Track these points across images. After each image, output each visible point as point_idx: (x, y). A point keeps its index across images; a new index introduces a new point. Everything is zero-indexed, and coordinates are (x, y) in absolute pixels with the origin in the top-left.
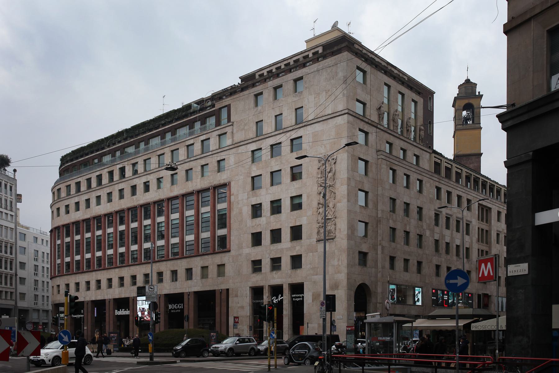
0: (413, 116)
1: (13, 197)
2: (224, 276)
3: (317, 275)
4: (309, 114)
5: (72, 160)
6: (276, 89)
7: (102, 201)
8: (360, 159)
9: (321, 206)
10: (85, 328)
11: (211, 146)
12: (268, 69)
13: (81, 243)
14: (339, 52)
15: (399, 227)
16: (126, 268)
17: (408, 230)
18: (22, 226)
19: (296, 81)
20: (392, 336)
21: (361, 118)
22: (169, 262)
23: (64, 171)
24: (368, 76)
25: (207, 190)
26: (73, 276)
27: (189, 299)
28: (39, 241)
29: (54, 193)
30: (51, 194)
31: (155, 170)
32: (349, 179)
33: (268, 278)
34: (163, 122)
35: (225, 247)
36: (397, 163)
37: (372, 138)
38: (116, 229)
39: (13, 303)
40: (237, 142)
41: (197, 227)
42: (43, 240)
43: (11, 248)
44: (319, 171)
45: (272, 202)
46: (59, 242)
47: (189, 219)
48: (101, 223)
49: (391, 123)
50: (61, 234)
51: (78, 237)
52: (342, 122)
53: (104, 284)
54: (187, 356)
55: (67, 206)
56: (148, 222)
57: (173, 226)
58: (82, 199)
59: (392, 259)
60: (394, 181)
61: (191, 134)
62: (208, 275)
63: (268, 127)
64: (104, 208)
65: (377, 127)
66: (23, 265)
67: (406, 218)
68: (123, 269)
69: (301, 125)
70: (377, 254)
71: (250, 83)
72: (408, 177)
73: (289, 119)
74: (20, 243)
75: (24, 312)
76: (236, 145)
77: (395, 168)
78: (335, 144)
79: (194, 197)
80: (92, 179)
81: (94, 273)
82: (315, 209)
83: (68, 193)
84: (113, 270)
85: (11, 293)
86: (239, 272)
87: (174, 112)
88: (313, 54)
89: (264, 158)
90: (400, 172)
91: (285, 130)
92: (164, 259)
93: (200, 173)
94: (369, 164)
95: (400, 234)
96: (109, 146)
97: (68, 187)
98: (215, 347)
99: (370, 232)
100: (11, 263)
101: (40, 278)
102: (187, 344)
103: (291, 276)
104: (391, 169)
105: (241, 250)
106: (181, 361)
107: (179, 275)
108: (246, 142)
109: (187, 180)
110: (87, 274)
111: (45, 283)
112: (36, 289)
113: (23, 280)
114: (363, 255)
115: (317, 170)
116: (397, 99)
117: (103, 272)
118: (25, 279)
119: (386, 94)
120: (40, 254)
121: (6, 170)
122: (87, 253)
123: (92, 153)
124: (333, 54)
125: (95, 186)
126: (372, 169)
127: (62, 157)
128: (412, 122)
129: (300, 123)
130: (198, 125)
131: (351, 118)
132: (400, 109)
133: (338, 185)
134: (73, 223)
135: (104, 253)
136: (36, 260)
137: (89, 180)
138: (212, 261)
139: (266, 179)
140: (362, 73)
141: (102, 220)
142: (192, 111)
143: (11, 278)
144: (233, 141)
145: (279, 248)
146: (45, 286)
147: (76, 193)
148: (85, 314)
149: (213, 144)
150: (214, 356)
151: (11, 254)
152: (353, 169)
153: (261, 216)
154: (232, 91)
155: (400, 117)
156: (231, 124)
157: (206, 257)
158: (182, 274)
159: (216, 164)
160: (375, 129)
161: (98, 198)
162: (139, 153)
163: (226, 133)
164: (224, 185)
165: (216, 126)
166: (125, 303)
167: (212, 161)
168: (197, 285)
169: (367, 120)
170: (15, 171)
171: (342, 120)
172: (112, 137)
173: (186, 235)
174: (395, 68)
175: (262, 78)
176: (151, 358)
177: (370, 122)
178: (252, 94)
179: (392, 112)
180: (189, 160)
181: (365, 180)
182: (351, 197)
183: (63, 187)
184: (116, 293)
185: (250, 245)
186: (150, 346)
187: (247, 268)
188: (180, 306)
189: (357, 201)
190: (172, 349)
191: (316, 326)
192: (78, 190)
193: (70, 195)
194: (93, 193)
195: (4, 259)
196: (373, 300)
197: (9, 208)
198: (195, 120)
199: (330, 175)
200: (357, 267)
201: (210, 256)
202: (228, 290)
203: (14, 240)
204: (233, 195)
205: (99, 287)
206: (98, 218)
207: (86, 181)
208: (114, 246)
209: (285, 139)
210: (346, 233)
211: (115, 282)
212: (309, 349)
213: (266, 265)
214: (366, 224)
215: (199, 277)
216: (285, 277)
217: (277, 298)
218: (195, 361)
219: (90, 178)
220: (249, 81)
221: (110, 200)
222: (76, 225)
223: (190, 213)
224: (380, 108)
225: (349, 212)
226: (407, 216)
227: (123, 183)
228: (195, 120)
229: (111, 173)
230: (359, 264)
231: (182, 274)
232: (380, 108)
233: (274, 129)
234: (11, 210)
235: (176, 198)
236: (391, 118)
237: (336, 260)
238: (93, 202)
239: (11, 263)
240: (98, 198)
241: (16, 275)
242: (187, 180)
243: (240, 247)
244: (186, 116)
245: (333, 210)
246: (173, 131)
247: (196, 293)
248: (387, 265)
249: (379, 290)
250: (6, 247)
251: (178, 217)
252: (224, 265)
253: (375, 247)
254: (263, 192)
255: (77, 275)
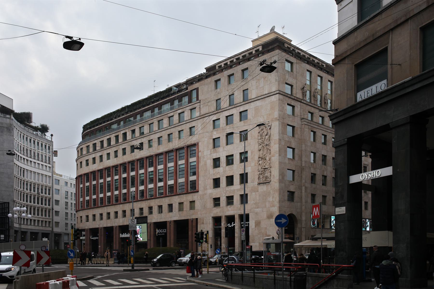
0: (329, 92)
1: (51, 154)
2: (194, 209)
3: (258, 208)
4: (252, 94)
5: (90, 128)
6: (229, 76)
7: (111, 157)
8: (288, 125)
9: (260, 159)
10: (100, 247)
11: (185, 117)
12: (225, 62)
13: (97, 186)
14: (273, 50)
15: (319, 173)
16: (128, 204)
17: (325, 175)
18: (57, 174)
19: (243, 71)
20: (280, 252)
21: (289, 96)
22: (157, 200)
23: (85, 136)
24: (294, 66)
25: (182, 148)
26: (91, 210)
27: (170, 226)
28: (69, 185)
29: (78, 151)
30: (76, 152)
31: (177, 125)
32: (280, 140)
33: (225, 211)
34: (153, 100)
35: (195, 189)
36: (316, 127)
37: (297, 110)
38: (120, 177)
39: (50, 229)
40: (203, 114)
41: (175, 174)
42: (71, 184)
43: (49, 190)
44: (259, 134)
45: (227, 157)
46: (81, 186)
47: (170, 169)
48: (110, 172)
49: (312, 98)
50: (83, 180)
51: (94, 183)
52: (275, 100)
53: (112, 215)
54: (160, 266)
55: (87, 161)
56: (142, 171)
57: (160, 174)
58: (97, 155)
59: (313, 196)
60: (314, 140)
61: (171, 109)
62: (183, 209)
63: (225, 104)
64: (112, 162)
65: (301, 102)
66: (57, 202)
67: (324, 166)
68: (125, 204)
69: (247, 102)
70: (302, 192)
71: (212, 72)
72: (325, 136)
73: (238, 97)
74: (56, 187)
75: (58, 235)
76: (202, 117)
77: (315, 130)
78: (270, 115)
79: (174, 154)
80: (136, 130)
81: (105, 208)
82: (257, 162)
83: (88, 151)
84: (118, 206)
85: (49, 222)
86: (204, 206)
87: (161, 93)
88: (256, 51)
89: (221, 126)
90: (319, 133)
91: (236, 106)
92: (153, 197)
93: (157, 142)
94: (296, 128)
95: (319, 179)
96: (115, 118)
97: (88, 147)
98: (180, 260)
99: (296, 177)
100: (49, 201)
101: (69, 211)
102: (160, 257)
103: (240, 209)
104: (312, 131)
105: (206, 190)
106: (154, 269)
107: (163, 209)
108: (209, 114)
109: (169, 141)
110: (100, 208)
111: (73, 215)
112: (66, 219)
113: (57, 213)
114: (291, 194)
115: (257, 134)
116: (317, 81)
117: (111, 207)
118: (59, 212)
119: (308, 78)
120: (69, 194)
121: (45, 135)
122: (100, 193)
123: (104, 122)
124: (269, 51)
125: (138, 135)
126: (298, 132)
127: (84, 126)
128: (329, 97)
129: (192, 119)
130: (176, 102)
131: (281, 97)
132: (319, 87)
133: (272, 144)
134: (91, 172)
135: (112, 193)
136: (67, 198)
137: (102, 142)
138: (186, 199)
139: (223, 140)
140: (290, 64)
141: (111, 170)
142: (172, 92)
143: (49, 212)
144: (200, 113)
145: (232, 189)
146: (73, 217)
147: (108, 146)
148: (100, 237)
149: (187, 116)
150: (180, 265)
151: (49, 194)
152: (283, 132)
153: (219, 166)
154: (200, 78)
155: (319, 93)
156: (199, 101)
157: (182, 196)
158: (165, 208)
159: (189, 130)
160: (300, 103)
161: (108, 154)
162: (136, 123)
163: (195, 108)
164: (194, 145)
165: (189, 103)
166: (124, 229)
167: (186, 128)
168: (176, 216)
169: (293, 97)
170: (52, 135)
171: (275, 98)
172: (118, 111)
173: (179, 178)
174: (316, 58)
175: (238, 61)
176: (133, 267)
177: (296, 98)
178: (213, 80)
179: (313, 90)
180: (170, 127)
181: (292, 140)
182: (282, 152)
183: (84, 146)
184: (121, 221)
185: (212, 187)
186: (132, 259)
187: (210, 204)
188: (164, 231)
189: (286, 155)
190: (151, 261)
191: (258, 244)
192: (95, 149)
193: (89, 153)
194: (105, 151)
195: (44, 198)
196: (299, 225)
197: (48, 162)
198: (174, 99)
199: (267, 137)
200: (287, 202)
201: (185, 195)
202: (197, 219)
203: (51, 185)
204: (200, 152)
205: (109, 218)
206: (108, 169)
207: (115, 138)
208: (119, 188)
209: (235, 112)
210: (278, 178)
211: (120, 214)
212: (235, 261)
213: (223, 201)
214: (294, 171)
215: (177, 210)
216: (235, 210)
217: (231, 225)
218: (162, 269)
219: (103, 141)
220: (212, 71)
221: (116, 156)
222: (93, 174)
223: (171, 165)
224: (303, 88)
225: (280, 163)
226: (325, 164)
227: (125, 144)
228: (174, 99)
229: (117, 137)
230: (288, 200)
231: (165, 208)
232: (303, 88)
233: (228, 105)
234: (49, 164)
235: (161, 154)
236: (312, 94)
237: (271, 197)
238: (105, 157)
239: (49, 201)
240: (108, 154)
241: (53, 209)
242: (169, 141)
243: (205, 189)
244: (168, 96)
245: (269, 162)
246: (160, 107)
247: (175, 221)
248: (309, 200)
249: (304, 218)
250: (46, 189)
251: (184, 163)
252: (194, 201)
253: (300, 188)
254: (220, 149)
255: (94, 209)
